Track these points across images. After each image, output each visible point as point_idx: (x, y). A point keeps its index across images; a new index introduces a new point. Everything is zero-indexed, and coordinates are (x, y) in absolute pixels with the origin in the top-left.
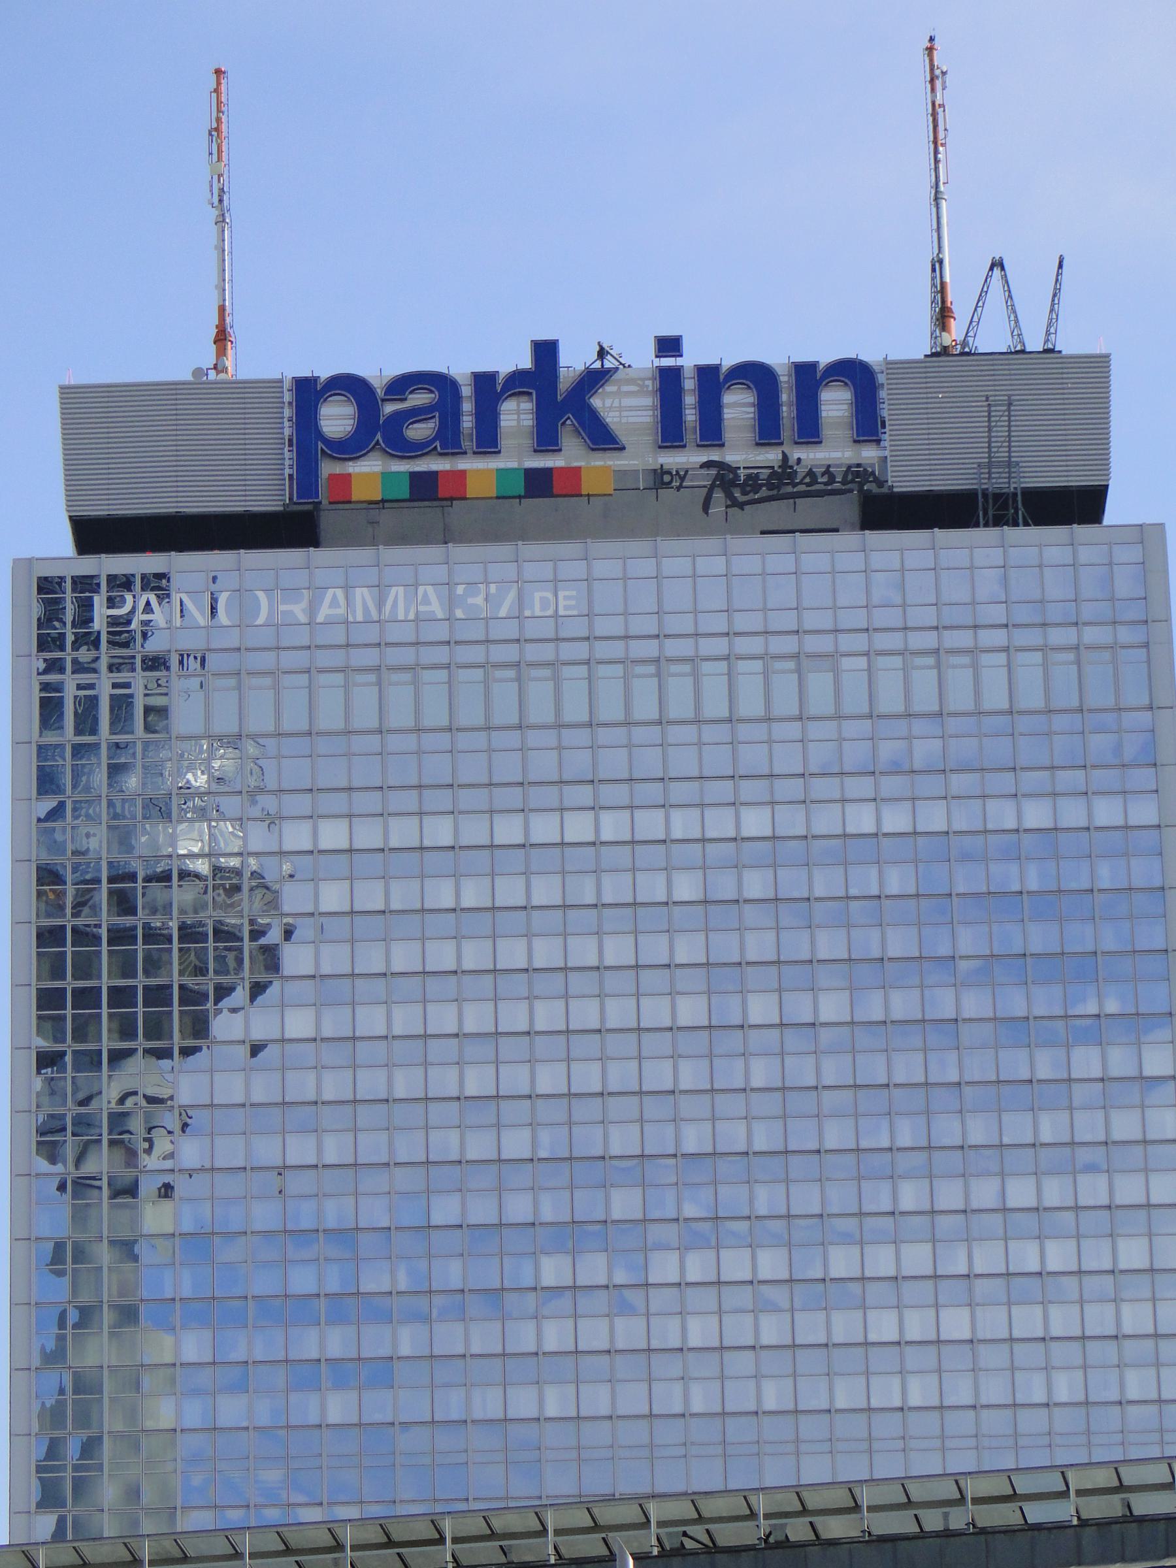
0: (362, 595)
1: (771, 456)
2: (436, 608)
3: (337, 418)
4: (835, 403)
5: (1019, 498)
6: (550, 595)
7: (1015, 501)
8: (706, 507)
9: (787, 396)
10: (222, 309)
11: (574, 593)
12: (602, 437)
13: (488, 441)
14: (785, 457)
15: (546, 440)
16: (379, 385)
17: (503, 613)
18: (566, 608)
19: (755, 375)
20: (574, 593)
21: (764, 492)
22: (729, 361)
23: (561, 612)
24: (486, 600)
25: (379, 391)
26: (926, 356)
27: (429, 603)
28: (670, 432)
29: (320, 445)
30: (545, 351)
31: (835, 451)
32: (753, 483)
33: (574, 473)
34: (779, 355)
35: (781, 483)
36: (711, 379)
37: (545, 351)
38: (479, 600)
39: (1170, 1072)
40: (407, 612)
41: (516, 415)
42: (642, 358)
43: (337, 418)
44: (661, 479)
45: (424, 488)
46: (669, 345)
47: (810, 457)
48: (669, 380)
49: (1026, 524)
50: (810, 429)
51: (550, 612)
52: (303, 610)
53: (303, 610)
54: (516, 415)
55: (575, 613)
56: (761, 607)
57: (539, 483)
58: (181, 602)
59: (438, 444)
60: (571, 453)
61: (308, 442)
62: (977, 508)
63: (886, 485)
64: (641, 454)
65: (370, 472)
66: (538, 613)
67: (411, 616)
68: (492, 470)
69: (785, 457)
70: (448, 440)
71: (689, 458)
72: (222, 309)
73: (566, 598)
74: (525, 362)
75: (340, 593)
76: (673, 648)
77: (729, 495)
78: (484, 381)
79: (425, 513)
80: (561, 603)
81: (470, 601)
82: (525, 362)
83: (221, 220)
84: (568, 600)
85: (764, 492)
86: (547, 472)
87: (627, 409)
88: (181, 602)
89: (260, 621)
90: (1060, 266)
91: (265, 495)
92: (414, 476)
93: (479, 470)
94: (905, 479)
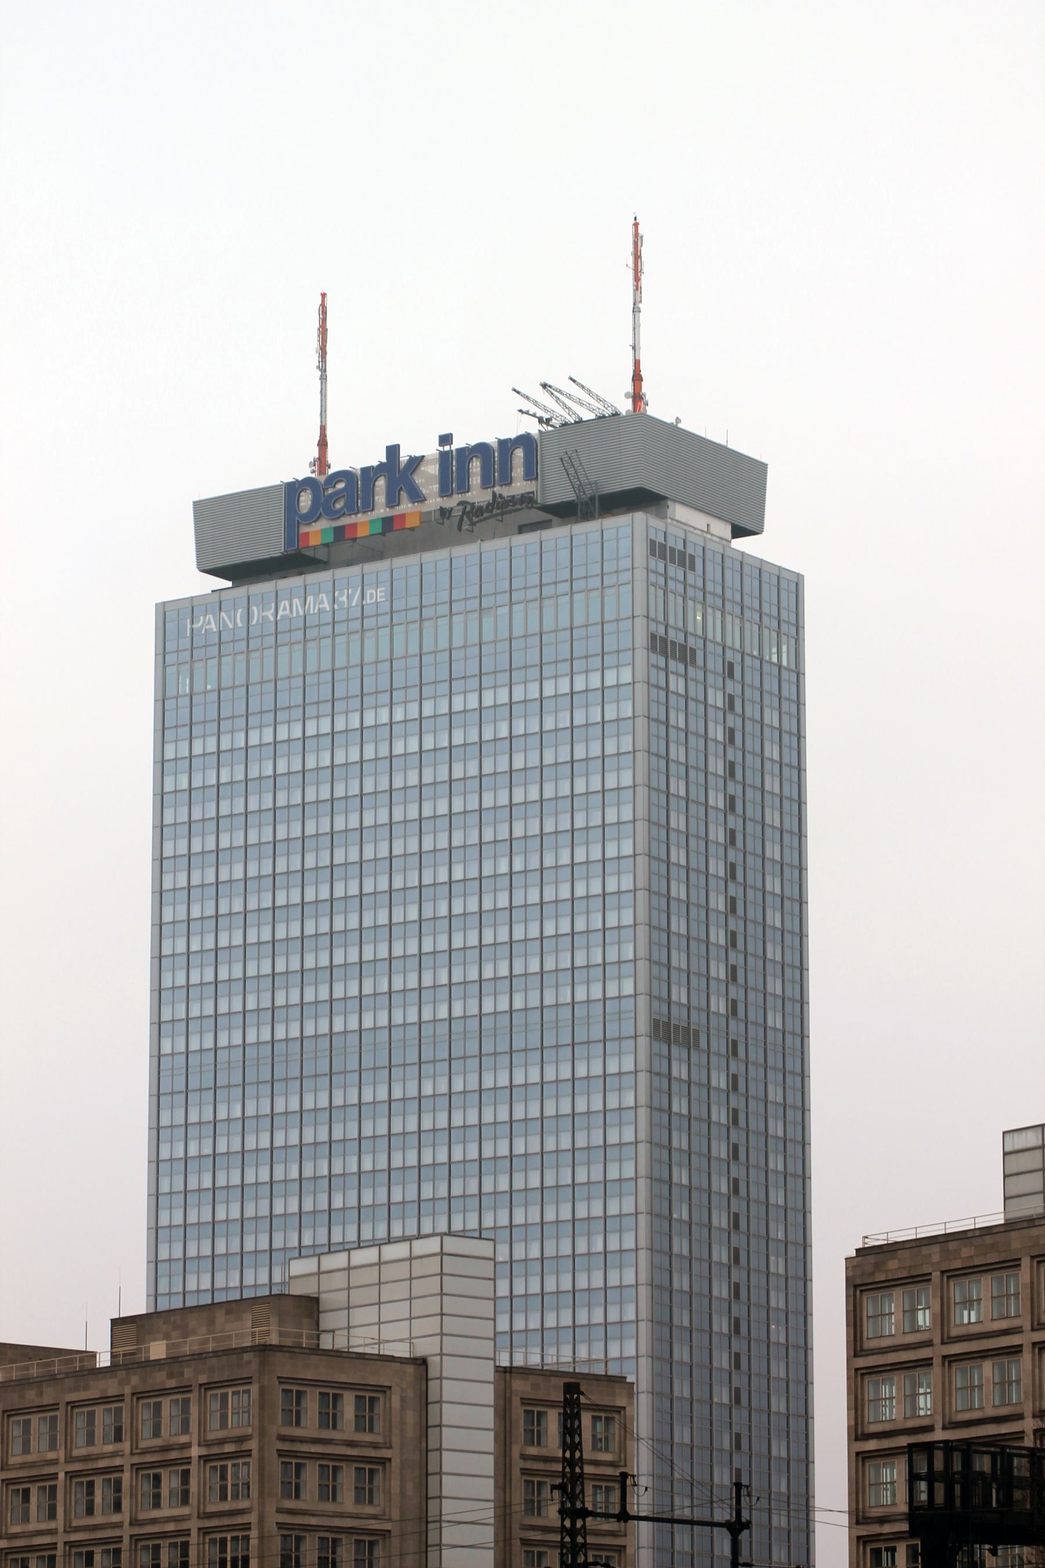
2: (327, 606)
3: (306, 501)
8: (460, 528)
9: (493, 458)
10: (323, 429)
12: (416, 496)
13: (369, 505)
14: (494, 494)
15: (392, 501)
19: (482, 449)
21: (485, 515)
22: (513, 436)
24: (348, 598)
28: (445, 491)
30: (393, 451)
31: (520, 486)
33: (403, 516)
35: (501, 507)
36: (466, 454)
37: (393, 451)
38: (344, 598)
39: (443, 1565)
42: (430, 448)
43: (306, 501)
44: (445, 513)
45: (340, 533)
46: (446, 439)
47: (506, 492)
48: (444, 458)
50: (507, 479)
57: (388, 523)
60: (406, 507)
61: (293, 519)
64: (434, 502)
69: (494, 494)
70: (351, 509)
72: (323, 429)
77: (470, 520)
78: (365, 471)
80: (379, 595)
87: (428, 478)
91: (274, 547)
93: (365, 522)
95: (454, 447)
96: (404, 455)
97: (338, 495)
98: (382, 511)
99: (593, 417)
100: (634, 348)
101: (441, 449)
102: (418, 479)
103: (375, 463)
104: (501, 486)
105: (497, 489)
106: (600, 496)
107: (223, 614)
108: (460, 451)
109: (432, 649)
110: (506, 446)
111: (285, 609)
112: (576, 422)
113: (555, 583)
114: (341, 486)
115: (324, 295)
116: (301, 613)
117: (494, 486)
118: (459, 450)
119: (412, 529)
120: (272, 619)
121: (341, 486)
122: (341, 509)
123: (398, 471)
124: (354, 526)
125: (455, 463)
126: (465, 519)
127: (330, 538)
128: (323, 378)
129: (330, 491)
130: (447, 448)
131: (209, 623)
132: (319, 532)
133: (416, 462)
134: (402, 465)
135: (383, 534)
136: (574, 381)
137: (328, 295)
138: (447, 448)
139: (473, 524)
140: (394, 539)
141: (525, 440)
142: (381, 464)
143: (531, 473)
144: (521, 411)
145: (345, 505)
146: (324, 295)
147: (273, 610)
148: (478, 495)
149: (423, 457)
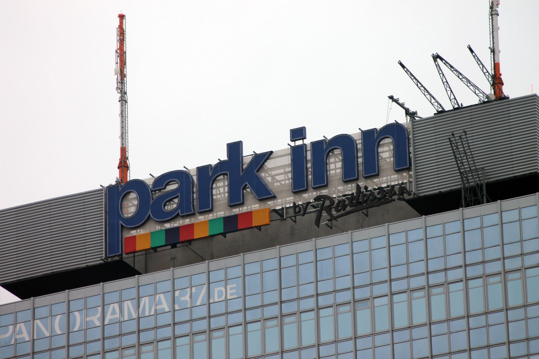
0: (129, 305)
1: (350, 189)
2: (165, 306)
3: (131, 206)
4: (386, 152)
5: (484, 188)
6: (223, 289)
7: (482, 190)
9: (357, 151)
10: (124, 150)
11: (235, 285)
12: (264, 193)
13: (207, 205)
14: (358, 187)
15: (235, 200)
16: (150, 182)
17: (198, 303)
18: (231, 294)
19: (343, 141)
20: (235, 285)
22: (379, 125)
23: (229, 297)
24: (191, 297)
25: (151, 186)
26: (435, 114)
27: (161, 304)
28: (299, 185)
29: (121, 222)
30: (235, 149)
31: (389, 179)
32: (341, 205)
33: (249, 214)
34: (353, 129)
36: (322, 148)
37: (235, 149)
38: (187, 298)
40: (150, 311)
41: (221, 190)
42: (282, 143)
43: (131, 206)
44: (299, 210)
45: (173, 238)
46: (298, 133)
47: (373, 184)
48: (297, 153)
49: (488, 202)
50: (373, 169)
51: (223, 298)
52: (98, 319)
53: (98, 319)
54: (221, 190)
55: (236, 296)
56: (519, 239)
57: (231, 224)
58: (128, 306)
59: (179, 211)
60: (252, 205)
61: (115, 224)
62: (461, 197)
63: (412, 193)
64: (285, 201)
65: (147, 235)
66: (216, 300)
67: (152, 313)
68: (220, 218)
69: (358, 187)
70: (186, 210)
71: (310, 196)
72: (124, 150)
73: (231, 289)
74: (224, 157)
75: (116, 306)
76: (434, 279)
78: (202, 170)
79: (178, 252)
80: (229, 292)
81: (182, 299)
82: (224, 157)
83: (123, 101)
84: (233, 290)
85: (348, 209)
86: (236, 217)
88: (128, 306)
89: (76, 329)
90: (403, 67)
91: (94, 255)
92: (168, 231)
93: (202, 223)
94: (431, 186)
95: (308, 141)
96: (248, 152)
97: (169, 197)
98: (221, 213)
99: (475, 100)
100: (493, 51)
101: (292, 144)
102: (266, 176)
103: (214, 162)
104: (366, 178)
105: (362, 184)
106: (489, 185)
107: (38, 322)
108: (316, 145)
109: (295, 345)
110: (372, 137)
111: (114, 312)
112: (455, 109)
113: (446, 270)
114: (173, 187)
115: (122, 17)
116: (135, 316)
117: (357, 179)
118: (314, 144)
119: (259, 228)
120: (98, 323)
121: (173, 187)
122: (175, 210)
123: (240, 169)
124: (191, 227)
125: (309, 158)
126: (324, 214)
127: (161, 241)
128: (123, 101)
129: (158, 194)
130: (299, 143)
131: (20, 332)
132: (147, 235)
133: (261, 159)
134: (247, 160)
135: (224, 234)
136: (472, 51)
137: (127, 17)
138: (299, 143)
139: (332, 218)
140: (238, 235)
141: (393, 130)
142: (221, 163)
143: (402, 163)
144: (391, 98)
145: (180, 206)
146: (122, 17)
147: (99, 315)
148: (338, 190)
149: (271, 152)
